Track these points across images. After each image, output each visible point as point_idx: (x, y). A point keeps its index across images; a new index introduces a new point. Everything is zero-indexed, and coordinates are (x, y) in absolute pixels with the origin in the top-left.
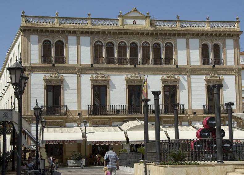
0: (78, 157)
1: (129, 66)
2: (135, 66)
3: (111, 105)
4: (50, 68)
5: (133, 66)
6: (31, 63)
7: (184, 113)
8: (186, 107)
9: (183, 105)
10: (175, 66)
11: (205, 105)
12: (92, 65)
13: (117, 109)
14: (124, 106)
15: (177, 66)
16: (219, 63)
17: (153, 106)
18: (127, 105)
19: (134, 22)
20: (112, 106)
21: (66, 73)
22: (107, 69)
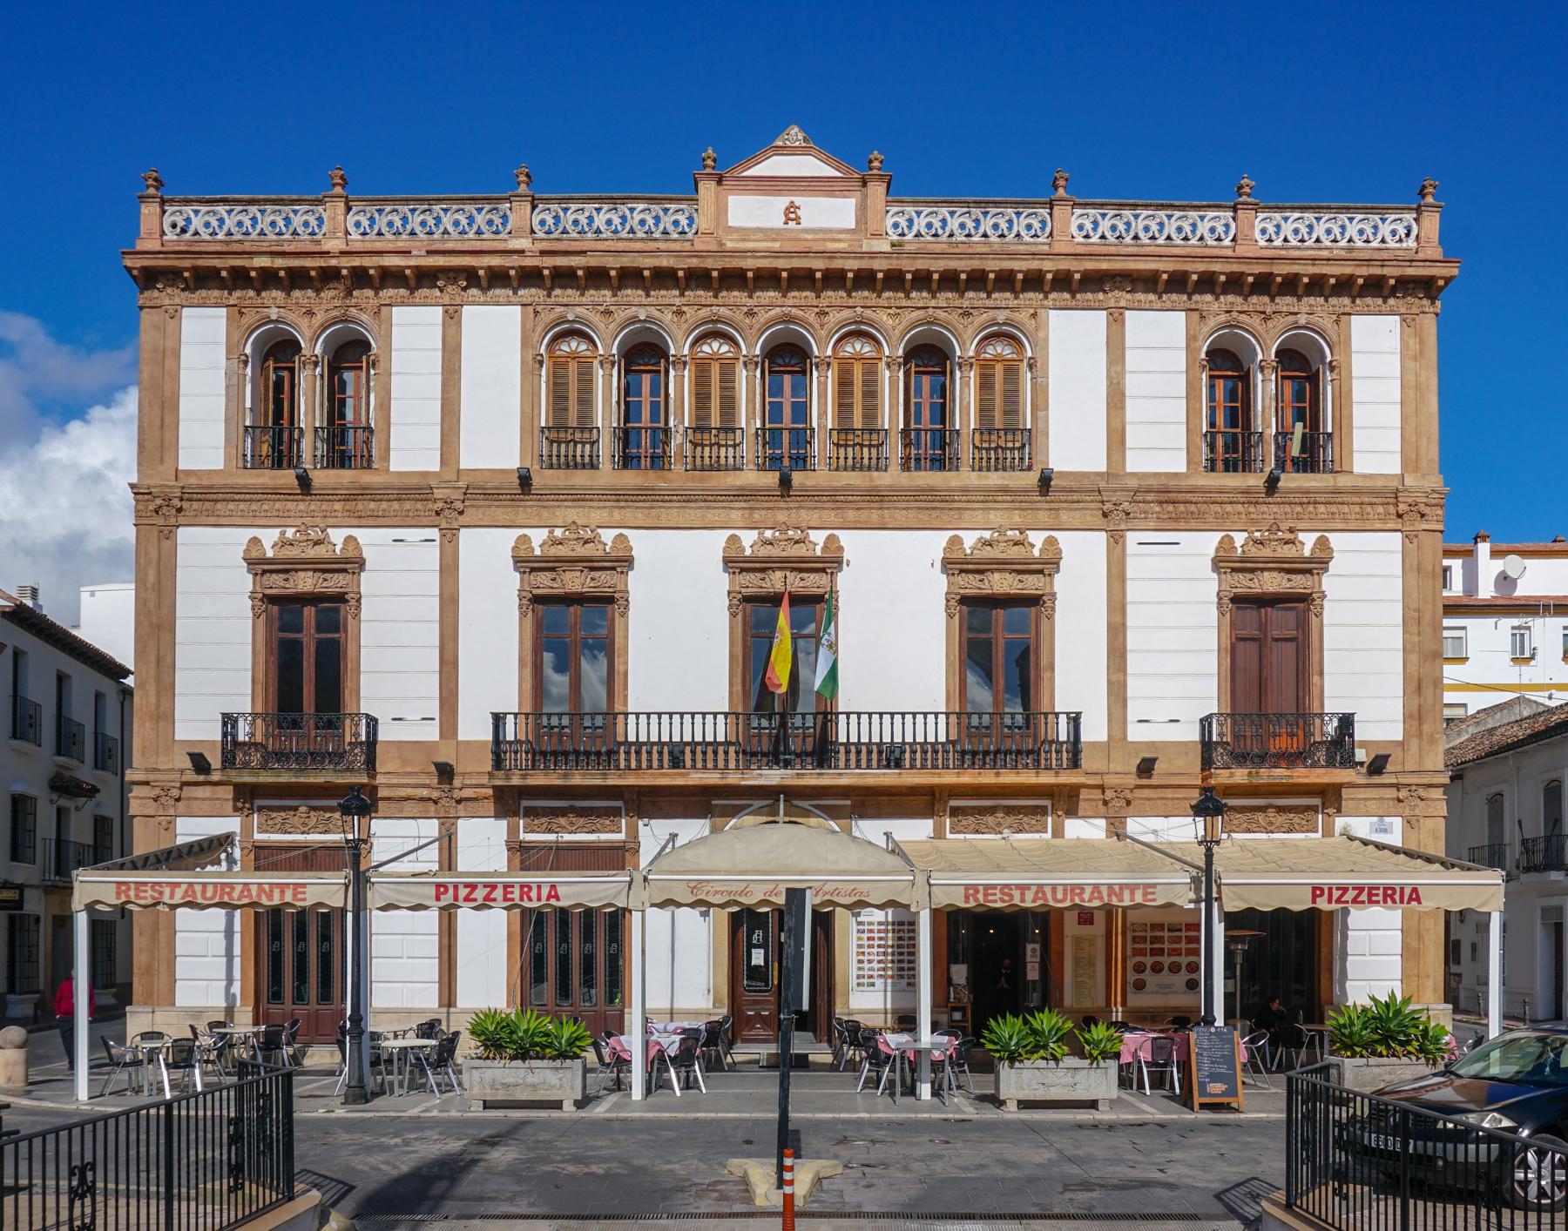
0: (893, 931)
1: (751, 477)
2: (785, 482)
3: (1057, 715)
4: (276, 493)
5: (771, 479)
6: (181, 467)
7: (1075, 763)
8: (1094, 731)
9: (1075, 720)
10: (1032, 478)
11: (1210, 716)
12: (525, 480)
13: (887, 739)
14: (931, 718)
15: (1045, 481)
16: (1310, 460)
17: (721, 718)
18: (947, 714)
19: (787, 211)
20: (632, 718)
21: (376, 521)
22: (619, 497)
